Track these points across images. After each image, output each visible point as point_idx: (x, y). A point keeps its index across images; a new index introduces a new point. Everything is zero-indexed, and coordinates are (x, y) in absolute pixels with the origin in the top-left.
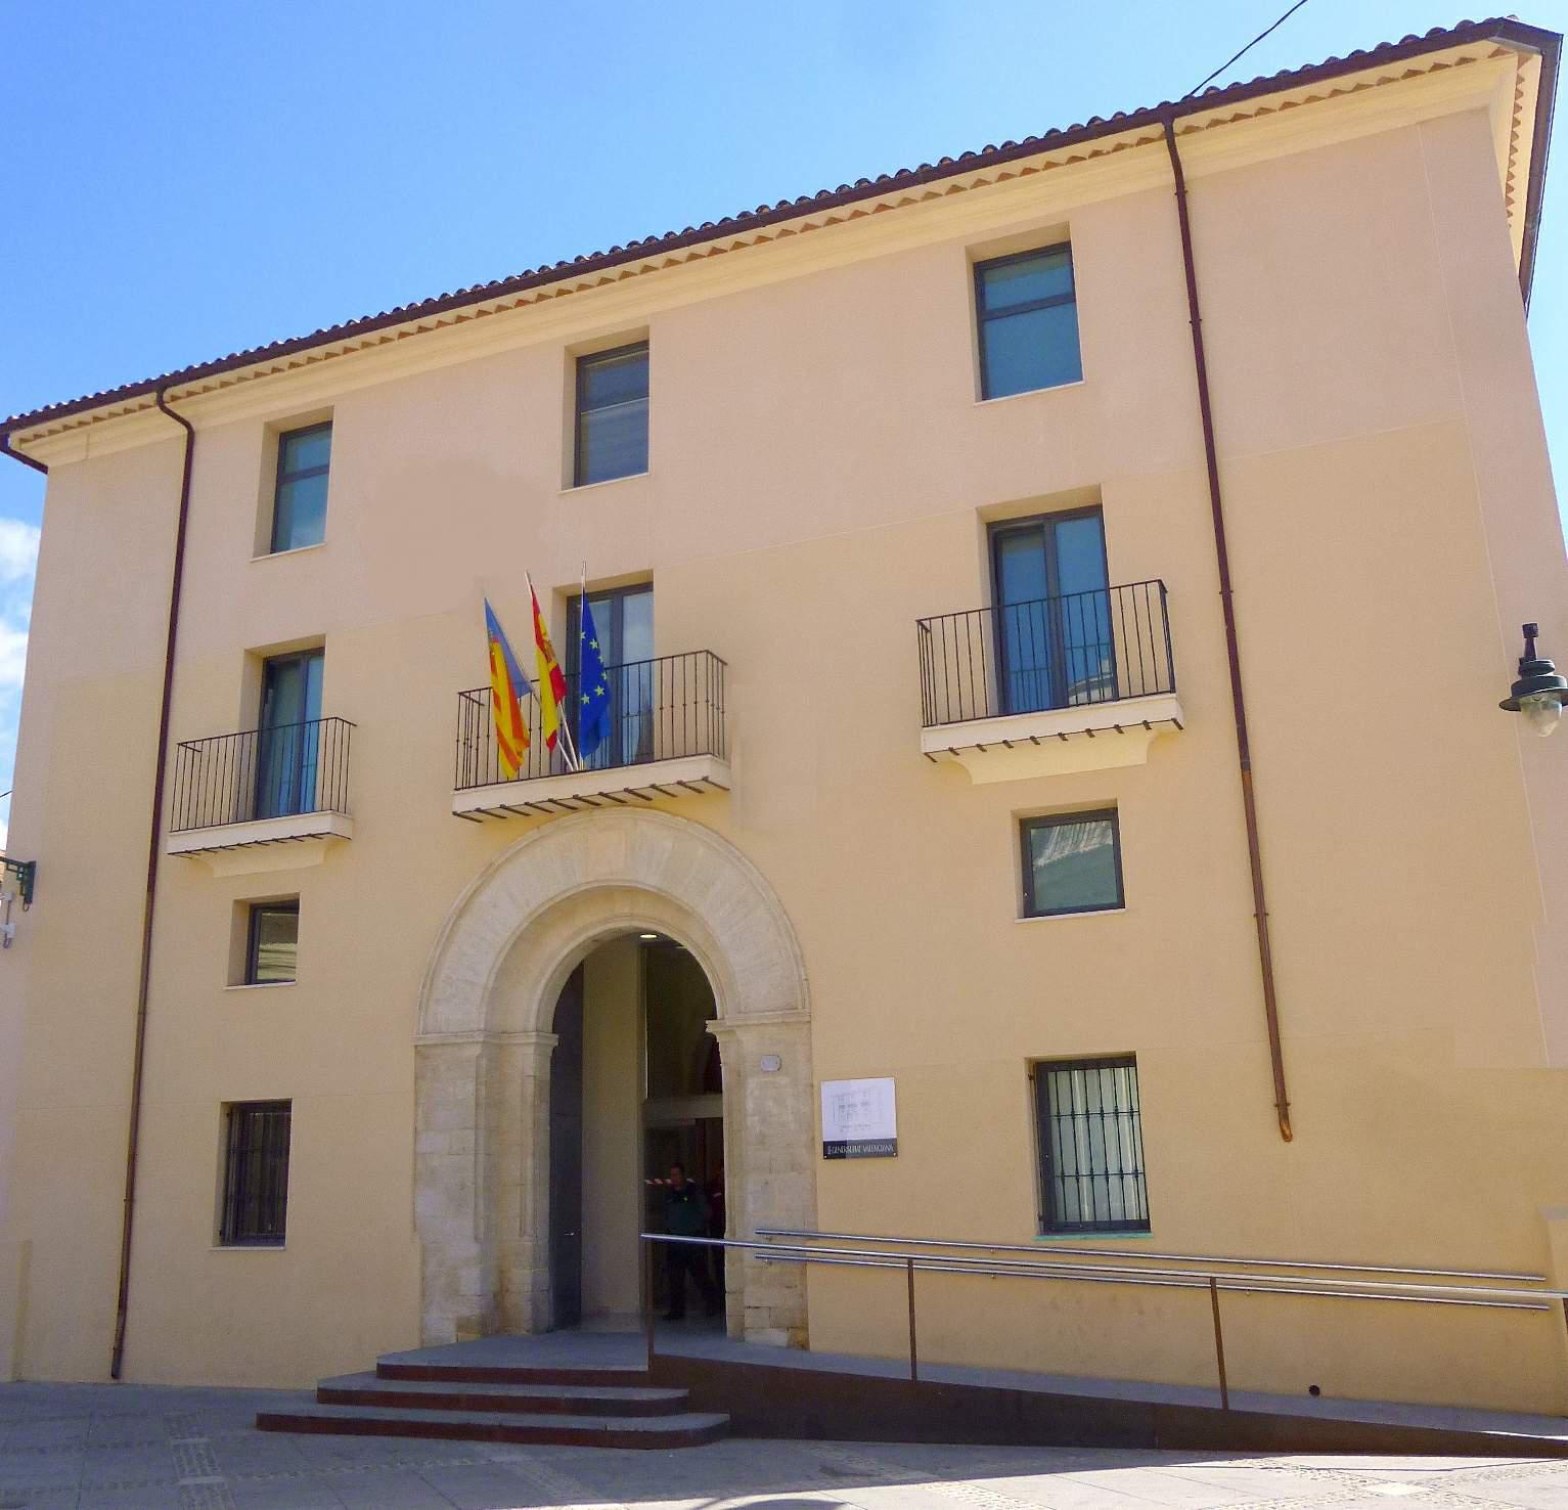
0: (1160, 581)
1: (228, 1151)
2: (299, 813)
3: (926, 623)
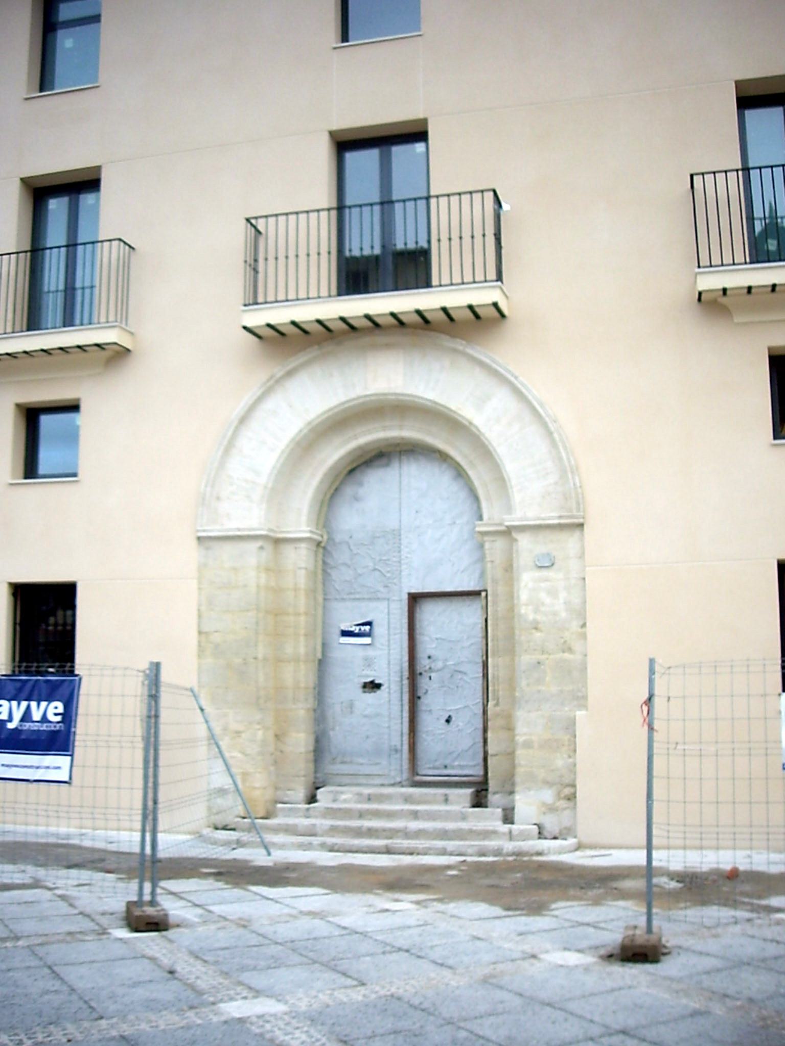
0: (494, 191)
1: (15, 624)
2: (72, 325)
3: (253, 221)
